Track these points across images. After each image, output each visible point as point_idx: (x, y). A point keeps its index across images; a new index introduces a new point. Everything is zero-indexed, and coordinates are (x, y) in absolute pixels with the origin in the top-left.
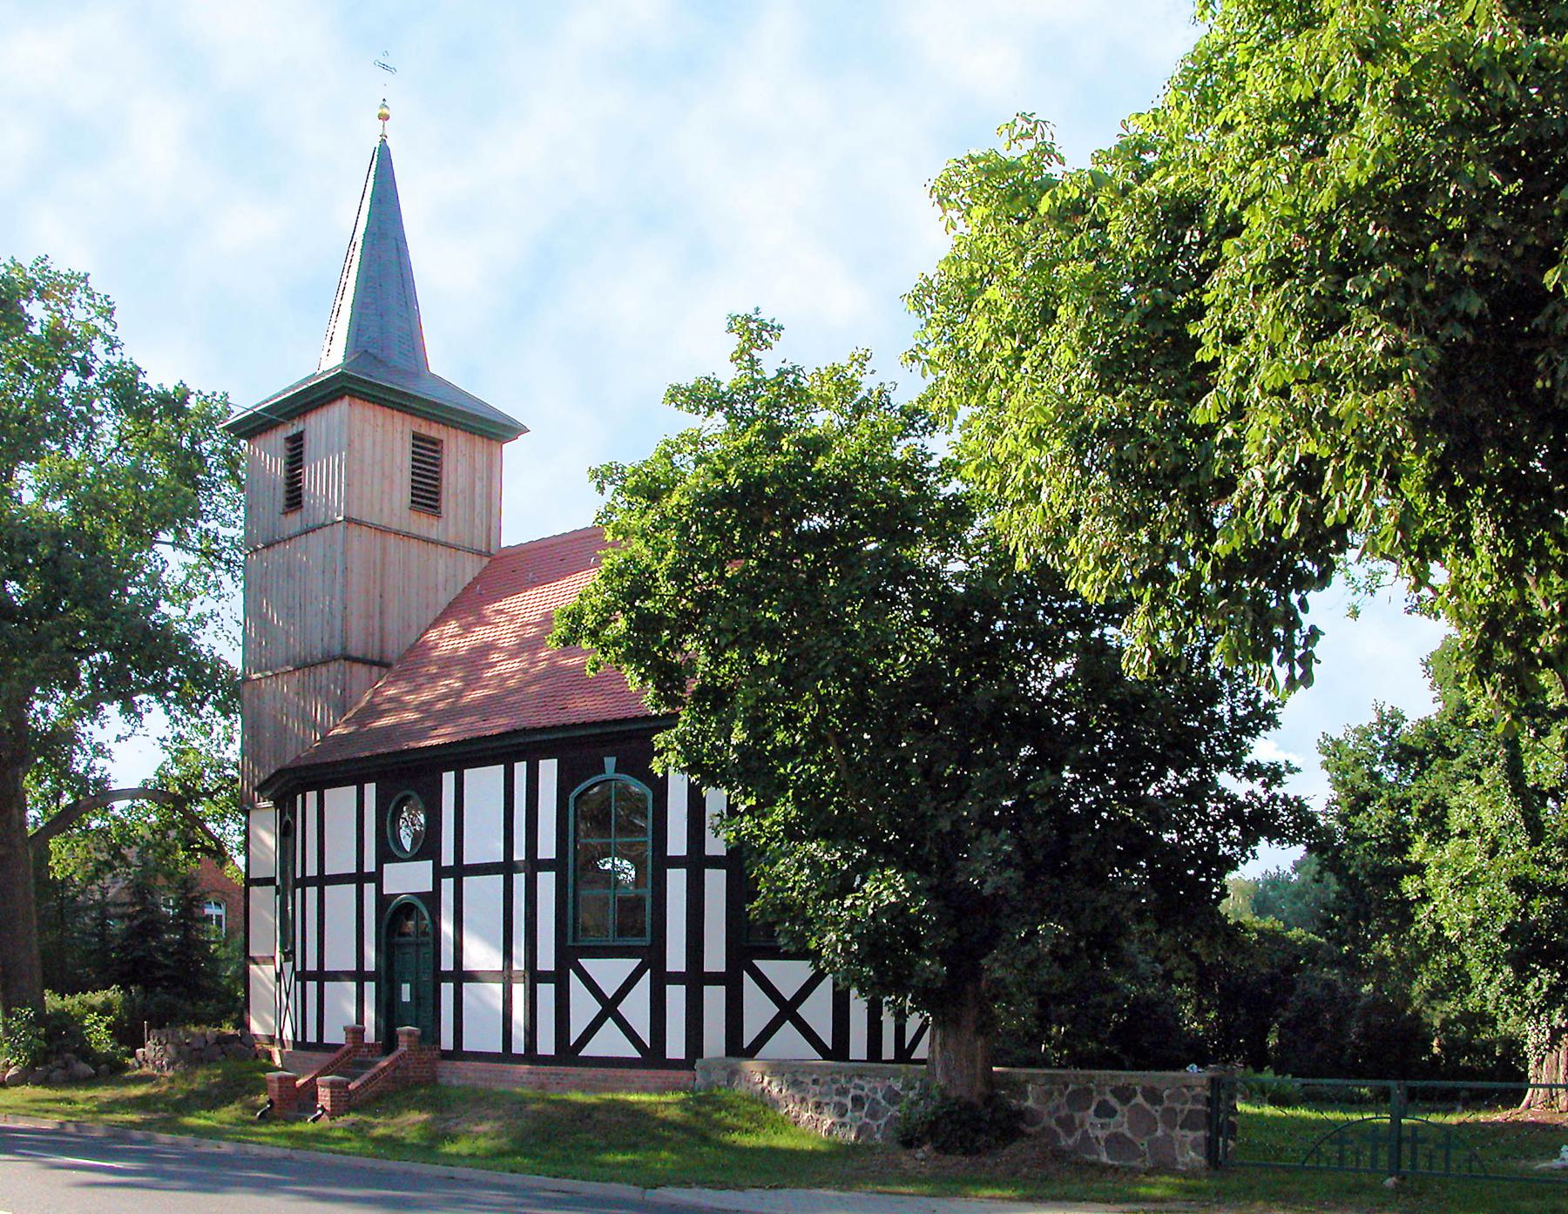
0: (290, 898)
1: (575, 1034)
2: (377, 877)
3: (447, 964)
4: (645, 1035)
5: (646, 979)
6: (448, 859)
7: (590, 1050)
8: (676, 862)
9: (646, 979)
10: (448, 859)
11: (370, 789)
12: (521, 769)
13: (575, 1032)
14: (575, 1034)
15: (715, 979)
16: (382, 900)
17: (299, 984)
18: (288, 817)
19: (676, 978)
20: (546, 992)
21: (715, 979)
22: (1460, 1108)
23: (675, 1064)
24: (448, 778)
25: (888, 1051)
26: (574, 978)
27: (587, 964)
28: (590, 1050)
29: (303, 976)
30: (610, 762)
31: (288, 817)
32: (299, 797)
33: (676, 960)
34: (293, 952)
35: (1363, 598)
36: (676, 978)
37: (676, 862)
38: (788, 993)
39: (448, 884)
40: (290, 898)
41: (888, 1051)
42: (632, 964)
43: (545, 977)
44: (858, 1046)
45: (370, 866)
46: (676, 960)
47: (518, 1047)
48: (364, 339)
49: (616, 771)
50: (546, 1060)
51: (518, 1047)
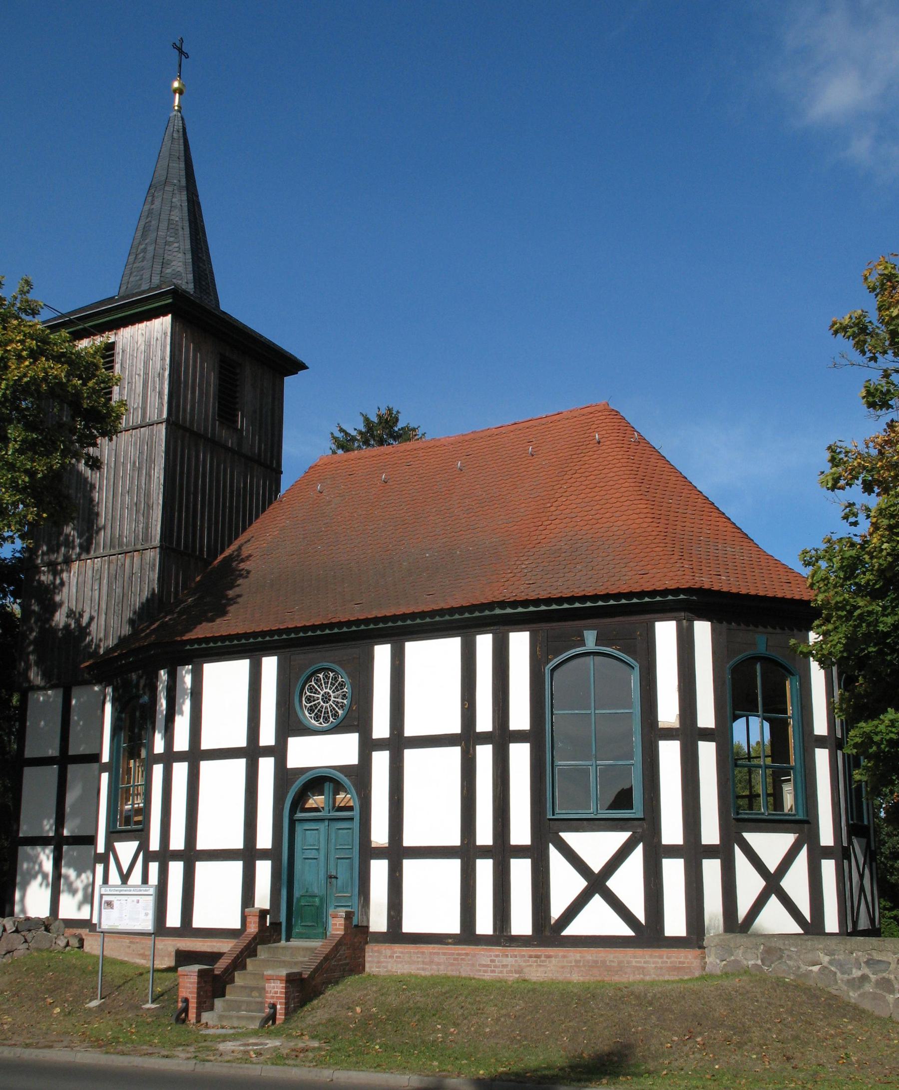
1: (556, 911)
2: (279, 752)
3: (380, 835)
4: (805, 908)
6: (381, 728)
7: (575, 928)
8: (669, 734)
9: (637, 856)
10: (381, 728)
11: (270, 665)
12: (484, 643)
13: (556, 911)
14: (556, 911)
15: (521, 852)
16: (283, 775)
21: (521, 852)
23: (676, 942)
24: (382, 653)
26: (554, 854)
27: (570, 838)
28: (575, 928)
32: (163, 675)
36: (673, 851)
38: (596, 865)
39: (381, 760)
42: (620, 838)
44: (832, 924)
45: (267, 737)
47: (485, 925)
48: (169, 271)
49: (596, 645)
51: (485, 925)
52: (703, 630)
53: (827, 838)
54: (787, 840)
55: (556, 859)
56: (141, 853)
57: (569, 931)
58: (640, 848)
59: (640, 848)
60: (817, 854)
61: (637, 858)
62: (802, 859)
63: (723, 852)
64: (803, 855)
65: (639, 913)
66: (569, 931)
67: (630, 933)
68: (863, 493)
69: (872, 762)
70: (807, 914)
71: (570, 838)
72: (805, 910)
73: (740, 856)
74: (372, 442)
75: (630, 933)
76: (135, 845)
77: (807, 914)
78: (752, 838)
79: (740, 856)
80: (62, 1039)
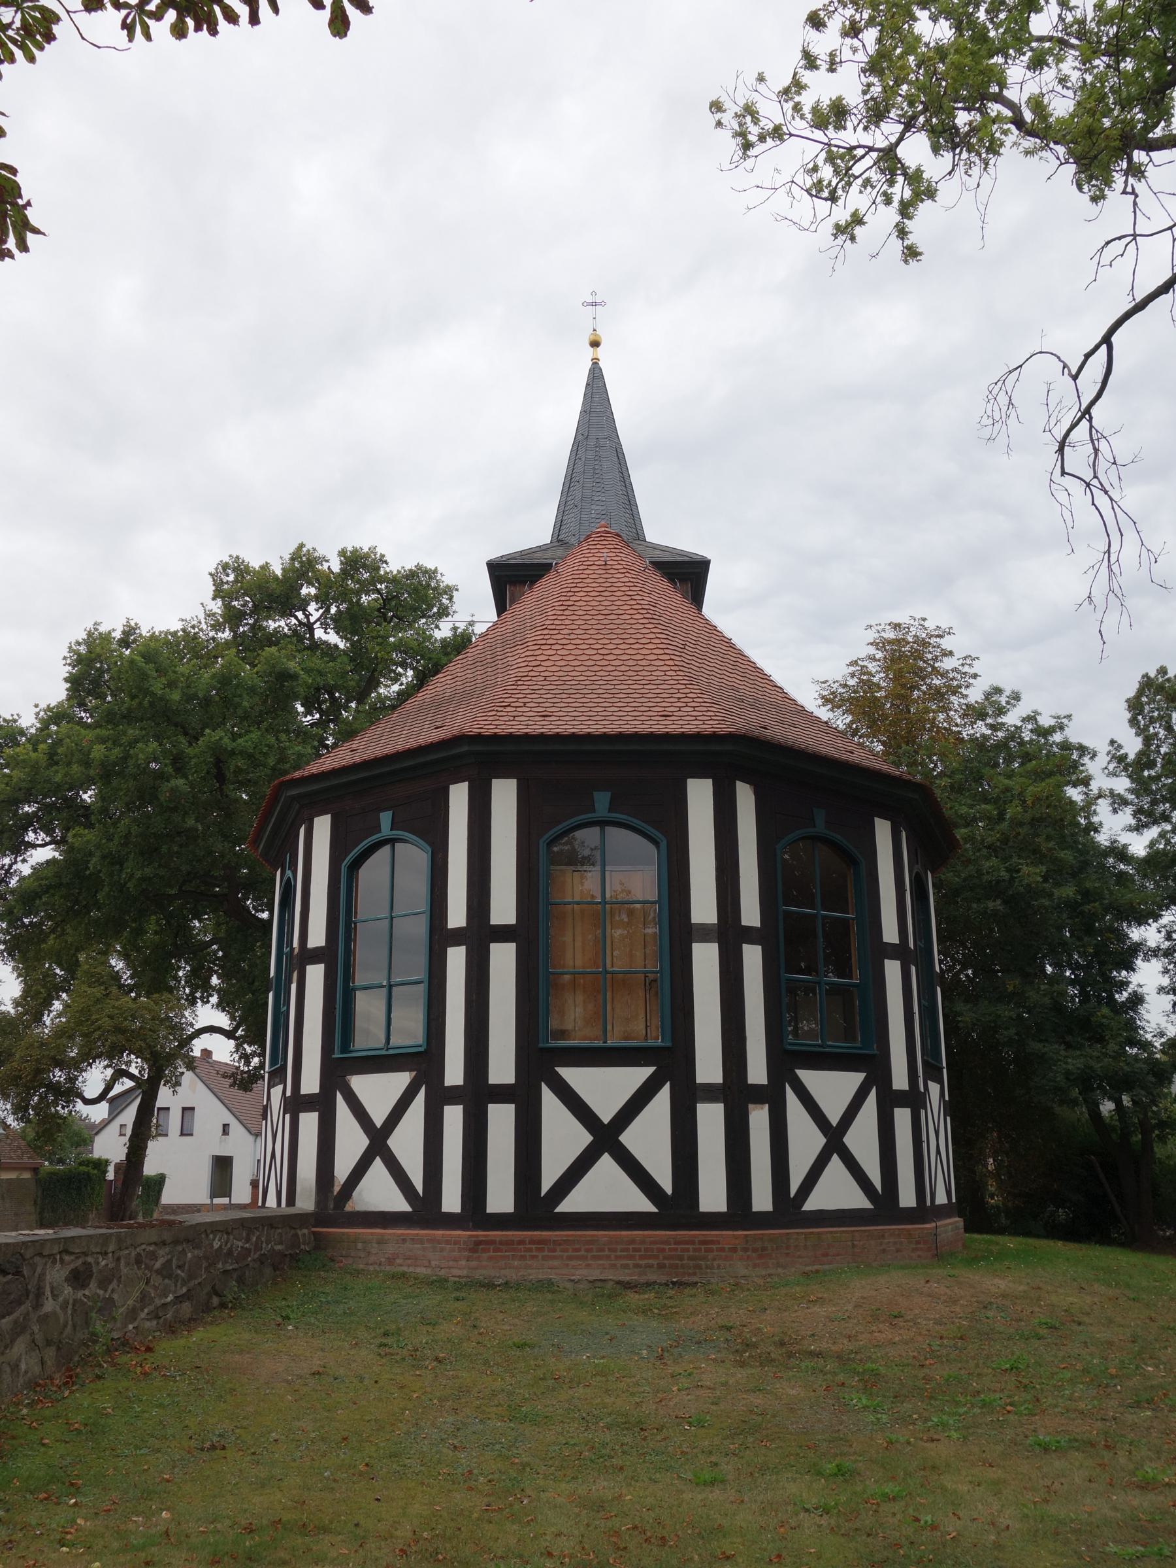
0: (294, 987)
1: (548, 1179)
4: (664, 1177)
5: (663, 1097)
7: (575, 1202)
9: (662, 1100)
13: (550, 1175)
15: (501, 1094)
17: (287, 1116)
18: (289, 873)
19: (710, 1093)
20: (309, 1122)
21: (501, 1094)
22: (61, 1224)
25: (762, 1199)
26: (549, 1100)
27: (571, 1075)
28: (575, 1202)
29: (439, 1098)
30: (386, 818)
31: (289, 873)
33: (454, 1074)
34: (284, 1067)
35: (37, 710)
36: (710, 1093)
37: (705, 933)
40: (294, 987)
41: (762, 1199)
42: (640, 1074)
43: (758, 1094)
46: (454, 1074)
49: (392, 829)
50: (501, 1221)
51: (452, 1200)
52: (745, 798)
53: (900, 1080)
54: (853, 1080)
55: (550, 1103)
56: (874, 1091)
57: (565, 1206)
58: (666, 1089)
59: (666, 1089)
60: (889, 1101)
61: (662, 1102)
62: (870, 1105)
63: (772, 1096)
64: (871, 1102)
65: (665, 1180)
66: (565, 1206)
67: (867, 1205)
68: (831, 99)
69: (1165, 1058)
70: (419, 1185)
71: (571, 1075)
72: (874, 1174)
73: (792, 1100)
74: (998, 844)
75: (867, 1205)
76: (400, 1080)
77: (419, 1185)
78: (808, 1077)
79: (792, 1100)
80: (463, 1295)
